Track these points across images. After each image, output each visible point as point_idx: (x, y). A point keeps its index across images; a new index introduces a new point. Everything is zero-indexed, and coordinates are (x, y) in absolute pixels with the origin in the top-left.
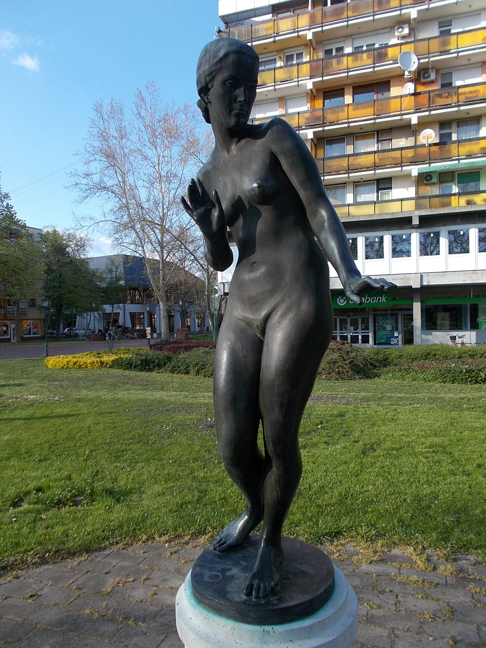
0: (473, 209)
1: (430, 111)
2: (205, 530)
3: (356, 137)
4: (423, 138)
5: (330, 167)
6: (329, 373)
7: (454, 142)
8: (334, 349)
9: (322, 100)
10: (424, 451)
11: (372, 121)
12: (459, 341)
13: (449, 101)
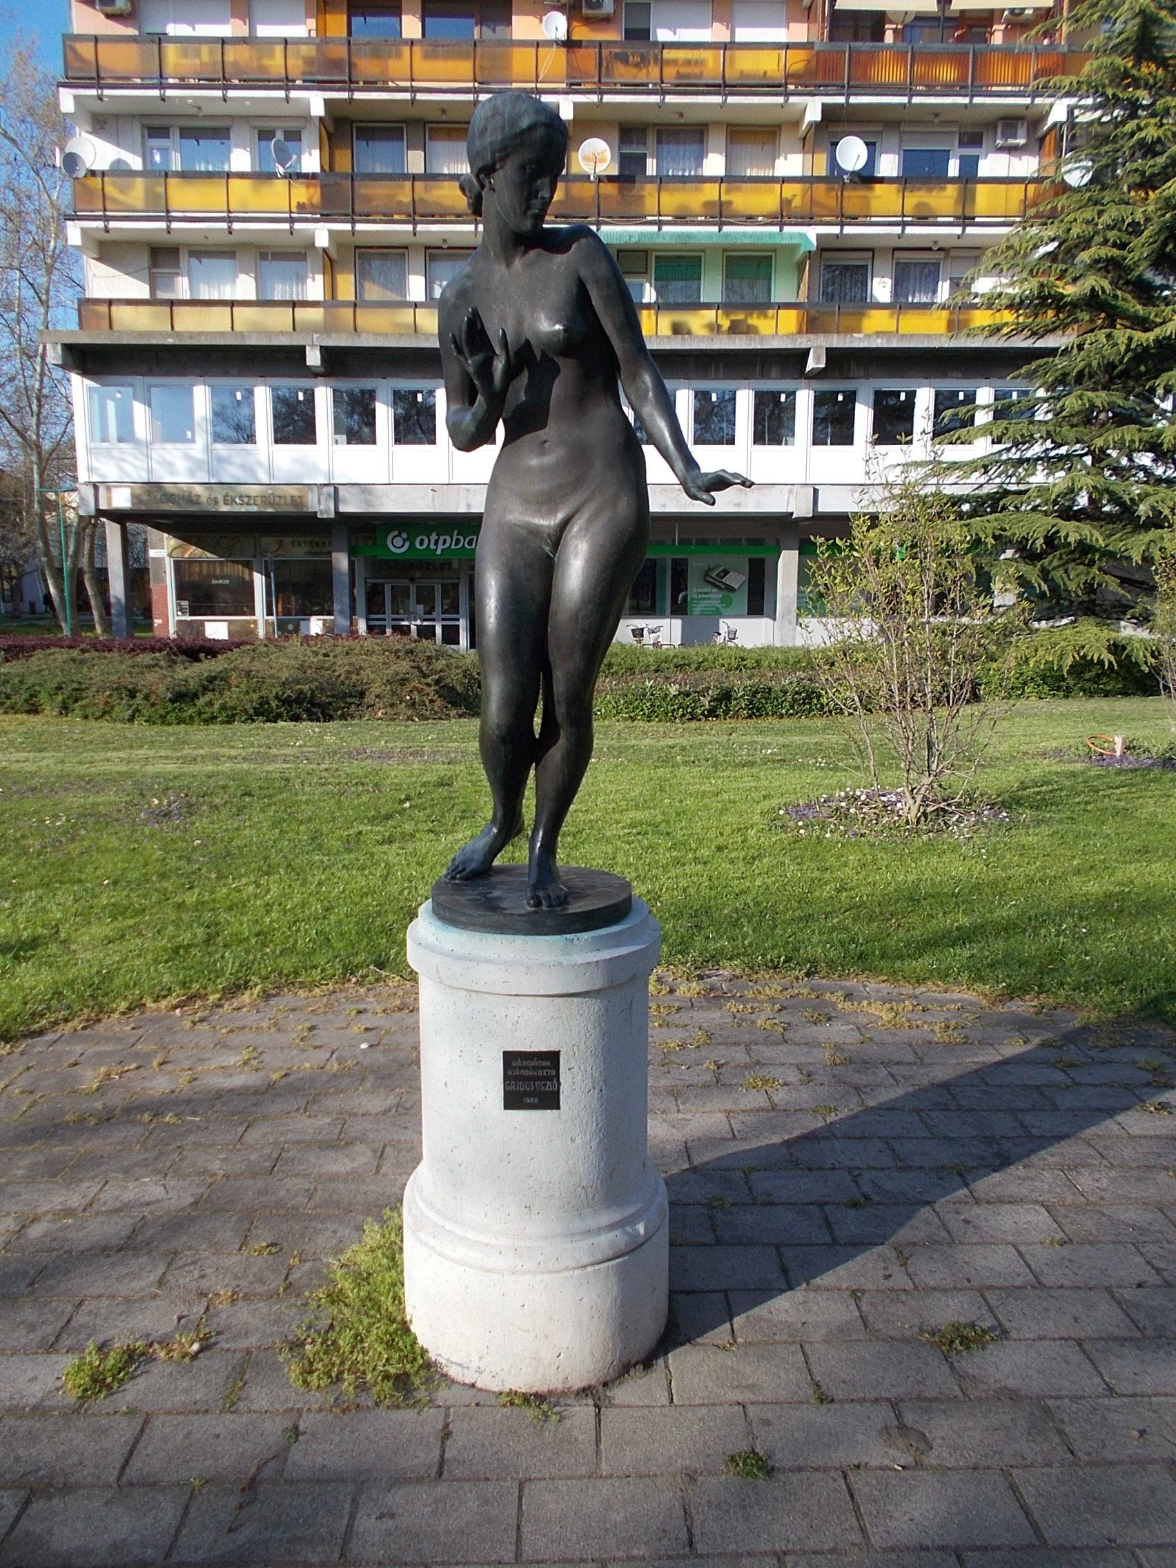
0: (687, 347)
1: (602, 93)
2: (247, 982)
3: (431, 129)
4: (586, 159)
5: (368, 199)
6: (392, 705)
7: (651, 180)
8: (398, 651)
9: (345, 17)
10: (622, 833)
11: (470, 97)
12: (648, 639)
13: (641, 77)
